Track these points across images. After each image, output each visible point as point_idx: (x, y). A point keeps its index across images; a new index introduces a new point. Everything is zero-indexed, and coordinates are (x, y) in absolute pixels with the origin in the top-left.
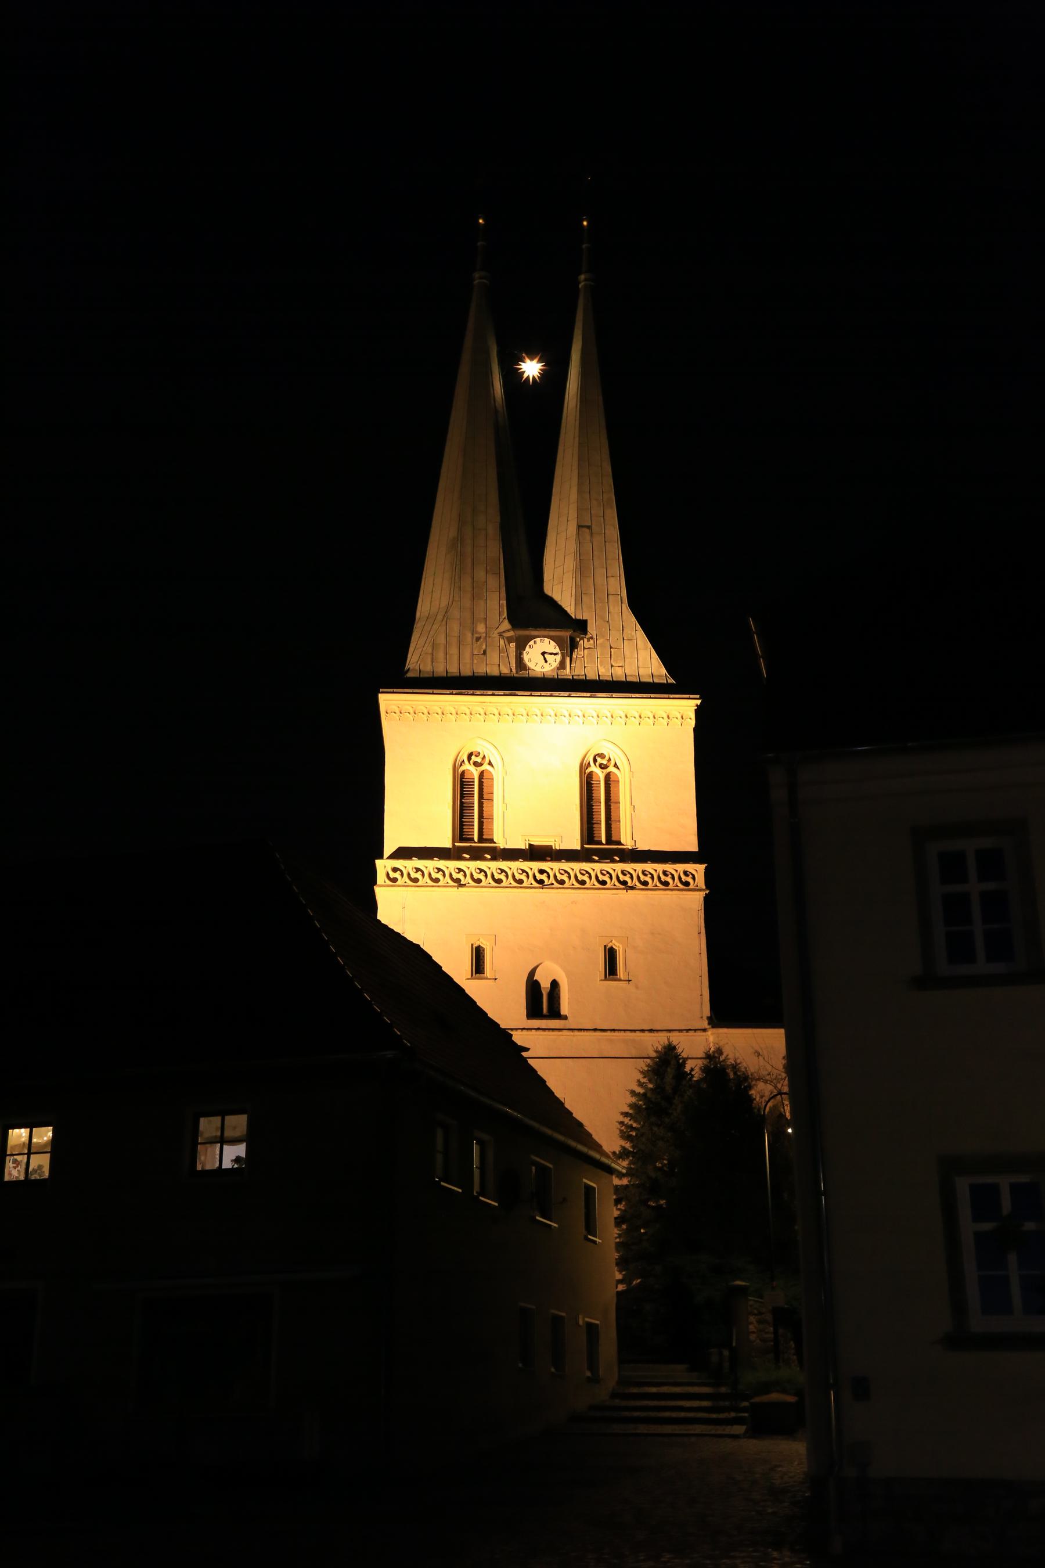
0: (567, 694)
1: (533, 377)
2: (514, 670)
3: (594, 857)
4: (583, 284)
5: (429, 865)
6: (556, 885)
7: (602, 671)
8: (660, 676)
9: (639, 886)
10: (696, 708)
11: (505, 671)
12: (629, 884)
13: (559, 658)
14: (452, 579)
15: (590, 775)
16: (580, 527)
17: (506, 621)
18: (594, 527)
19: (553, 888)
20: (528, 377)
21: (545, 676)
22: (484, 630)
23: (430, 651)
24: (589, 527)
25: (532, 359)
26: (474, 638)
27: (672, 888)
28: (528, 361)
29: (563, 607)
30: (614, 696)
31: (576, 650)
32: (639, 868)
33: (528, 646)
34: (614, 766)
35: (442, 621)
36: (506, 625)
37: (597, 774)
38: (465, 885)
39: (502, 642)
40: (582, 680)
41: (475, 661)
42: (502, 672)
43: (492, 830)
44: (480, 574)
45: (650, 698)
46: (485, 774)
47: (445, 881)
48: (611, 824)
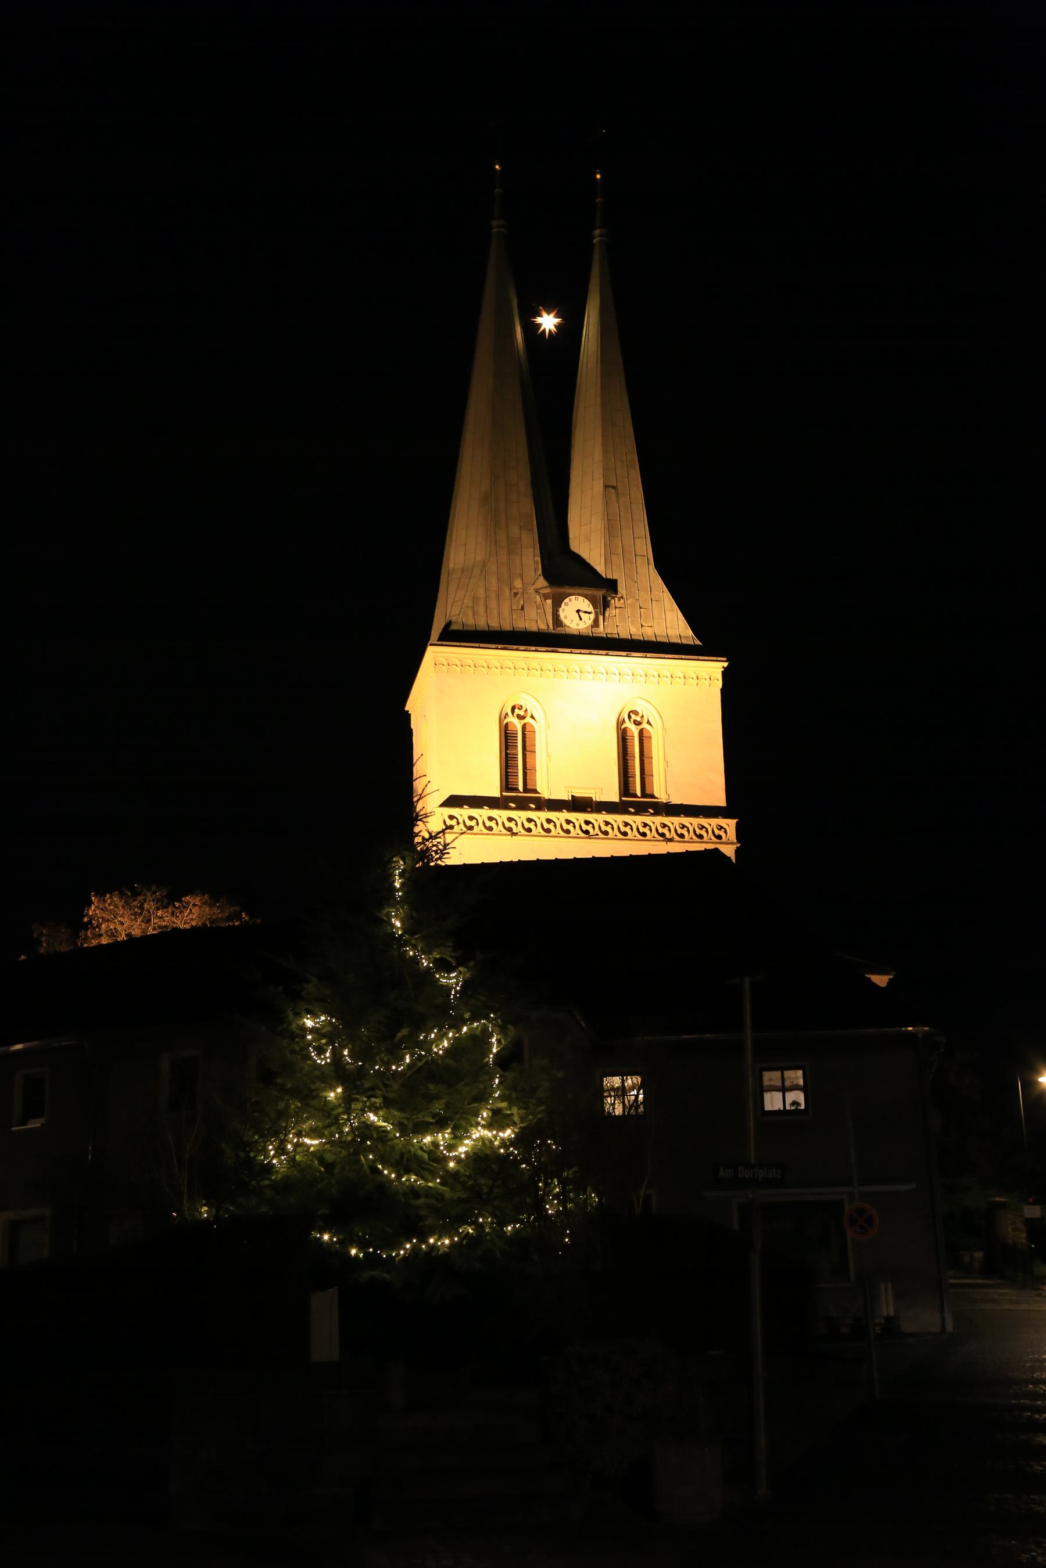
0: (605, 652)
1: (550, 331)
2: (551, 627)
3: (631, 809)
4: (598, 239)
5: (483, 813)
6: (601, 835)
7: (633, 630)
8: (686, 637)
9: (676, 838)
10: (723, 670)
11: (543, 627)
12: (514, 831)
13: (592, 616)
14: (487, 531)
15: (625, 730)
16: (606, 487)
17: (542, 578)
18: (619, 488)
19: (599, 839)
20: (544, 330)
21: (502, 629)
22: (521, 586)
23: (471, 604)
24: (614, 488)
25: (549, 314)
26: (512, 594)
27: (496, 833)
28: (545, 315)
29: (592, 565)
30: (648, 656)
31: (608, 609)
32: (638, 820)
33: (563, 603)
34: (647, 723)
35: (481, 575)
36: (542, 582)
37: (631, 730)
38: (517, 833)
39: (538, 598)
40: (616, 639)
41: (514, 616)
42: (540, 628)
43: (535, 780)
44: (515, 530)
45: (682, 659)
46: (527, 727)
47: (576, 832)
48: (644, 778)
